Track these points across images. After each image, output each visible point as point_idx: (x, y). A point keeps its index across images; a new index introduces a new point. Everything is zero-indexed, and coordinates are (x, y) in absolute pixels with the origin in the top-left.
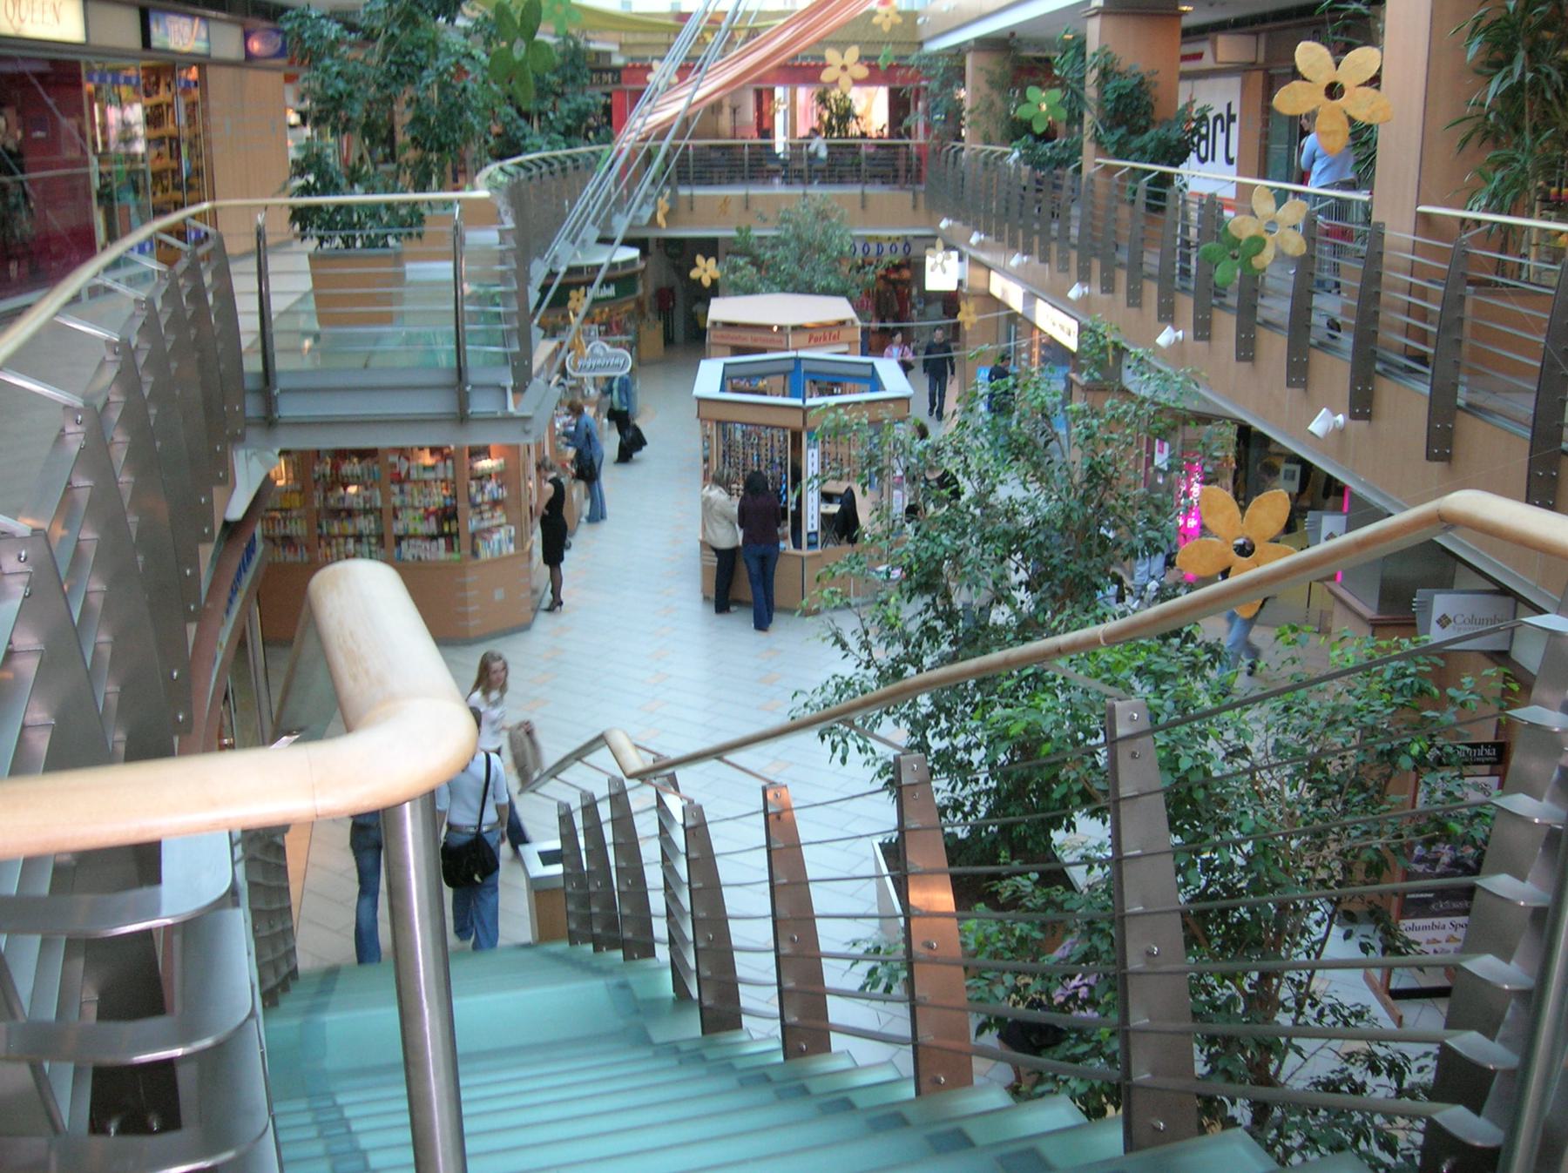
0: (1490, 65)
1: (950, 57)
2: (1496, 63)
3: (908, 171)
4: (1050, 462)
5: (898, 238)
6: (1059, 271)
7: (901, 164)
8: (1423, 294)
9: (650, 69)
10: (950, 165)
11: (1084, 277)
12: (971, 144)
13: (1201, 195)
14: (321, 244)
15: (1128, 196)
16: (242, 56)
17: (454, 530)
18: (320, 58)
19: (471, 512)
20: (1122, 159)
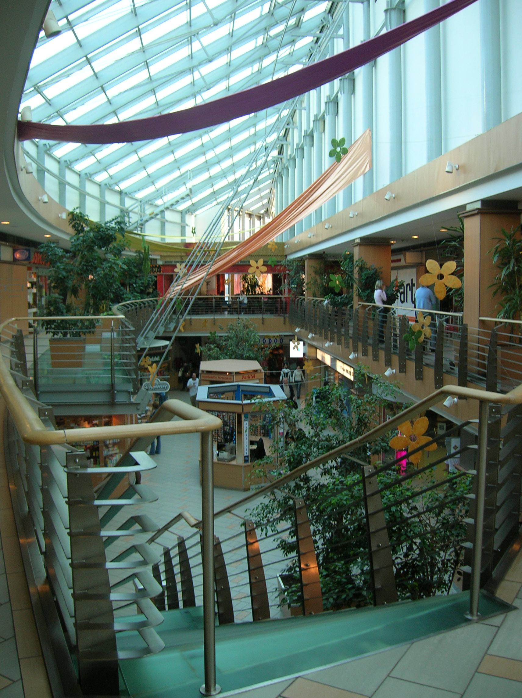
0: (502, 264)
1: (298, 261)
2: (504, 263)
3: (281, 308)
4: (343, 418)
5: (278, 336)
6: (345, 348)
7: (278, 305)
8: (483, 350)
9: (175, 266)
10: (299, 306)
11: (355, 350)
12: (308, 297)
13: (400, 316)
14: (53, 336)
15: (372, 317)
16: (12, 260)
17: (97, 455)
18: (55, 262)
19: (104, 448)
20: (369, 302)
